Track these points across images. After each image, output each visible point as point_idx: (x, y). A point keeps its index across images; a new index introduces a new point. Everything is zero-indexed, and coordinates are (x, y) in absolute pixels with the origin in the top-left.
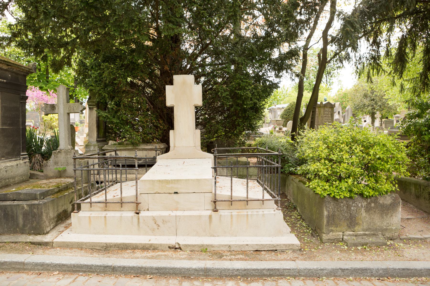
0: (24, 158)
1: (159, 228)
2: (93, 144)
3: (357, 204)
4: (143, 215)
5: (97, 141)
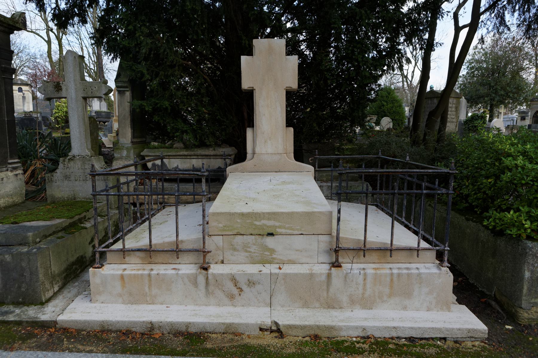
0: (15, 169)
1: (242, 293)
2: (126, 146)
4: (215, 272)
5: (132, 142)
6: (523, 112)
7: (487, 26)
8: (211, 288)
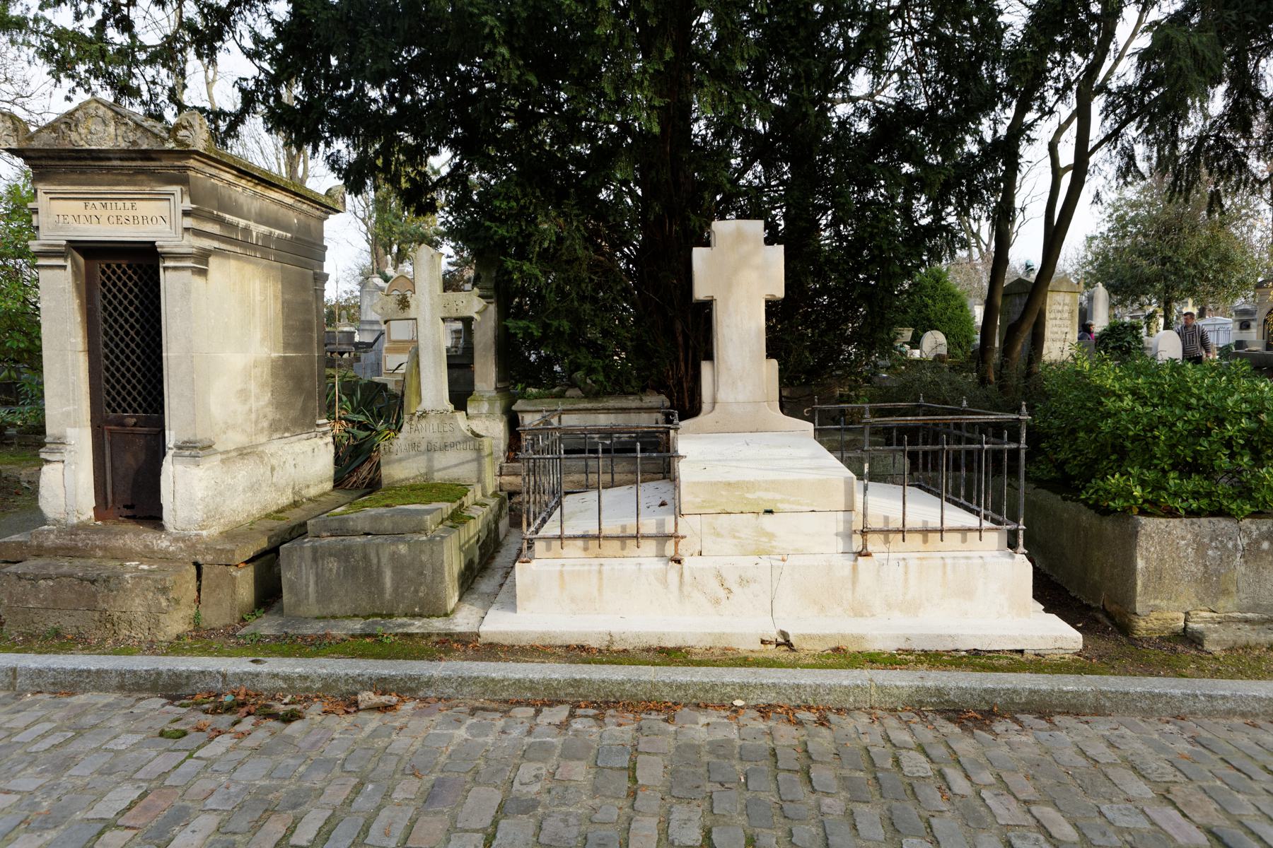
1: (731, 596)
2: (488, 395)
3: (1221, 542)
6: (1245, 312)
7: (1104, 174)
8: (687, 589)
